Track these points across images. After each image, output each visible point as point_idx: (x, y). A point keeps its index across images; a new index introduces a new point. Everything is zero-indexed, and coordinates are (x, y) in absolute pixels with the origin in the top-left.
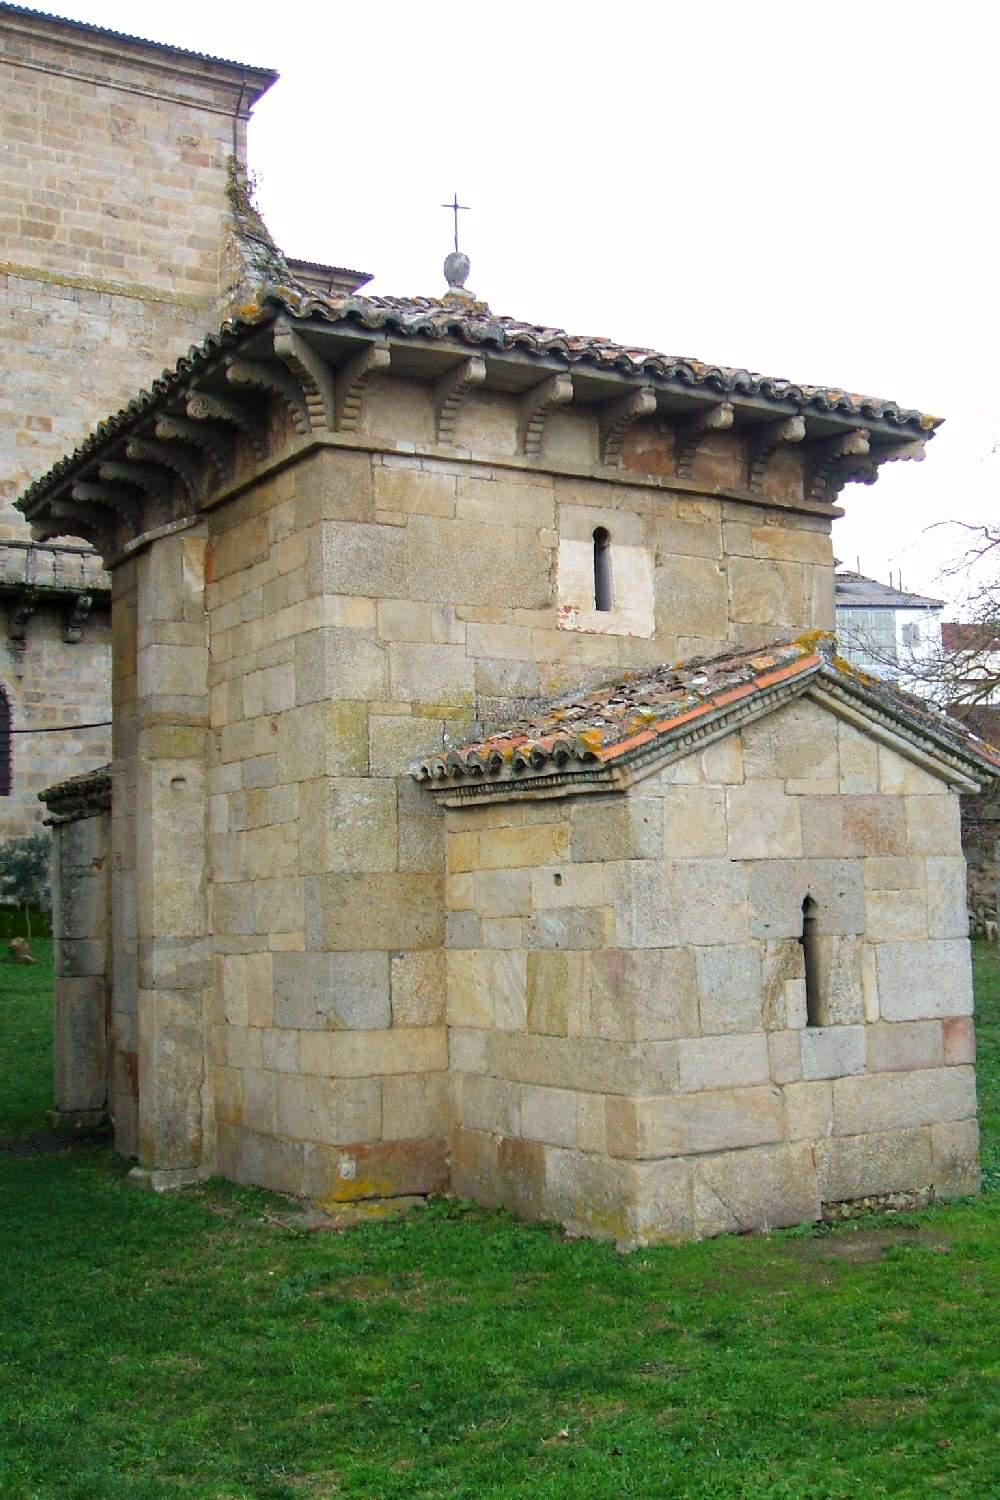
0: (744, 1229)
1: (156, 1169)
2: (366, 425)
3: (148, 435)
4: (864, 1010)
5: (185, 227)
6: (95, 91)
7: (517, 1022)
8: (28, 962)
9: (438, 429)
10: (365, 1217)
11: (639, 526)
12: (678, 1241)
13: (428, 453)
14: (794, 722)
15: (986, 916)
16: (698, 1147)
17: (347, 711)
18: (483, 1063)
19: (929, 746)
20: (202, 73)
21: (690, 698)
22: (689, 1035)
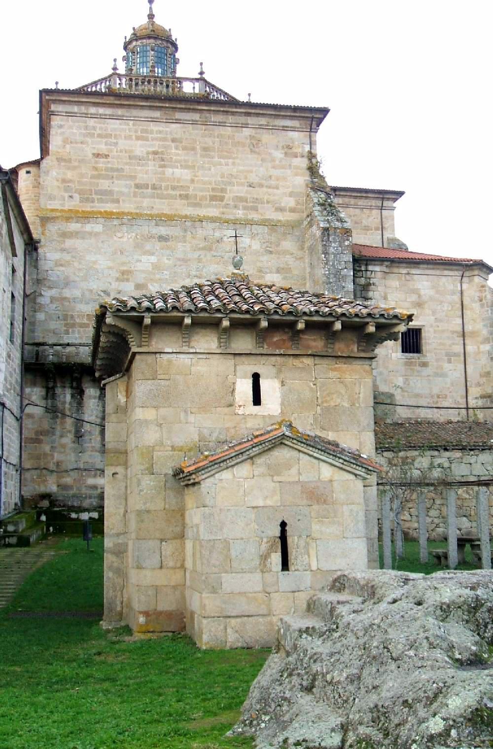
2: (153, 343)
4: (310, 566)
5: (287, 188)
6: (242, 131)
11: (274, 370)
16: (229, 614)
17: (145, 451)
19: (341, 461)
20: (292, 114)
22: (226, 572)
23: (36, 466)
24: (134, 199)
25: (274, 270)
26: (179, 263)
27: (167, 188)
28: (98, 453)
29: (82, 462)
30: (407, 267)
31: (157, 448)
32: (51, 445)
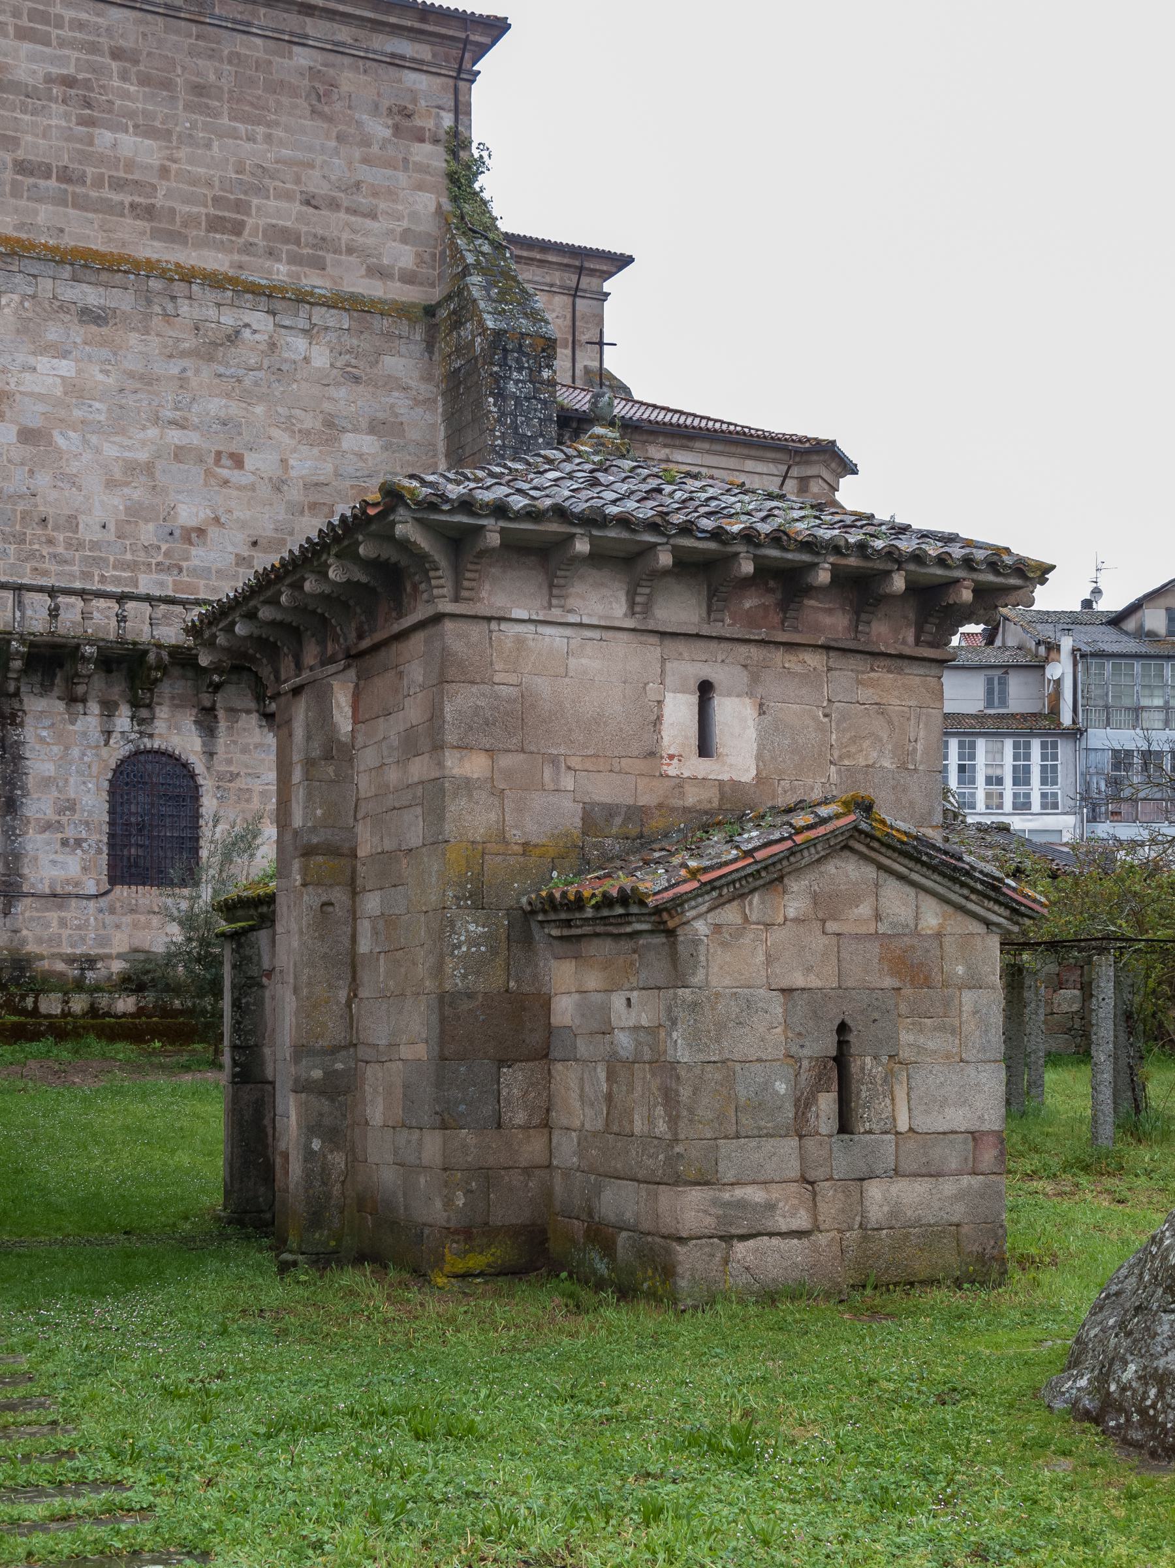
2: (484, 594)
6: (290, 53)
9: (551, 595)
11: (744, 677)
13: (541, 618)
14: (833, 871)
24: (13, 201)
25: (364, 425)
26: (131, 384)
27: (98, 183)
30: (665, 446)
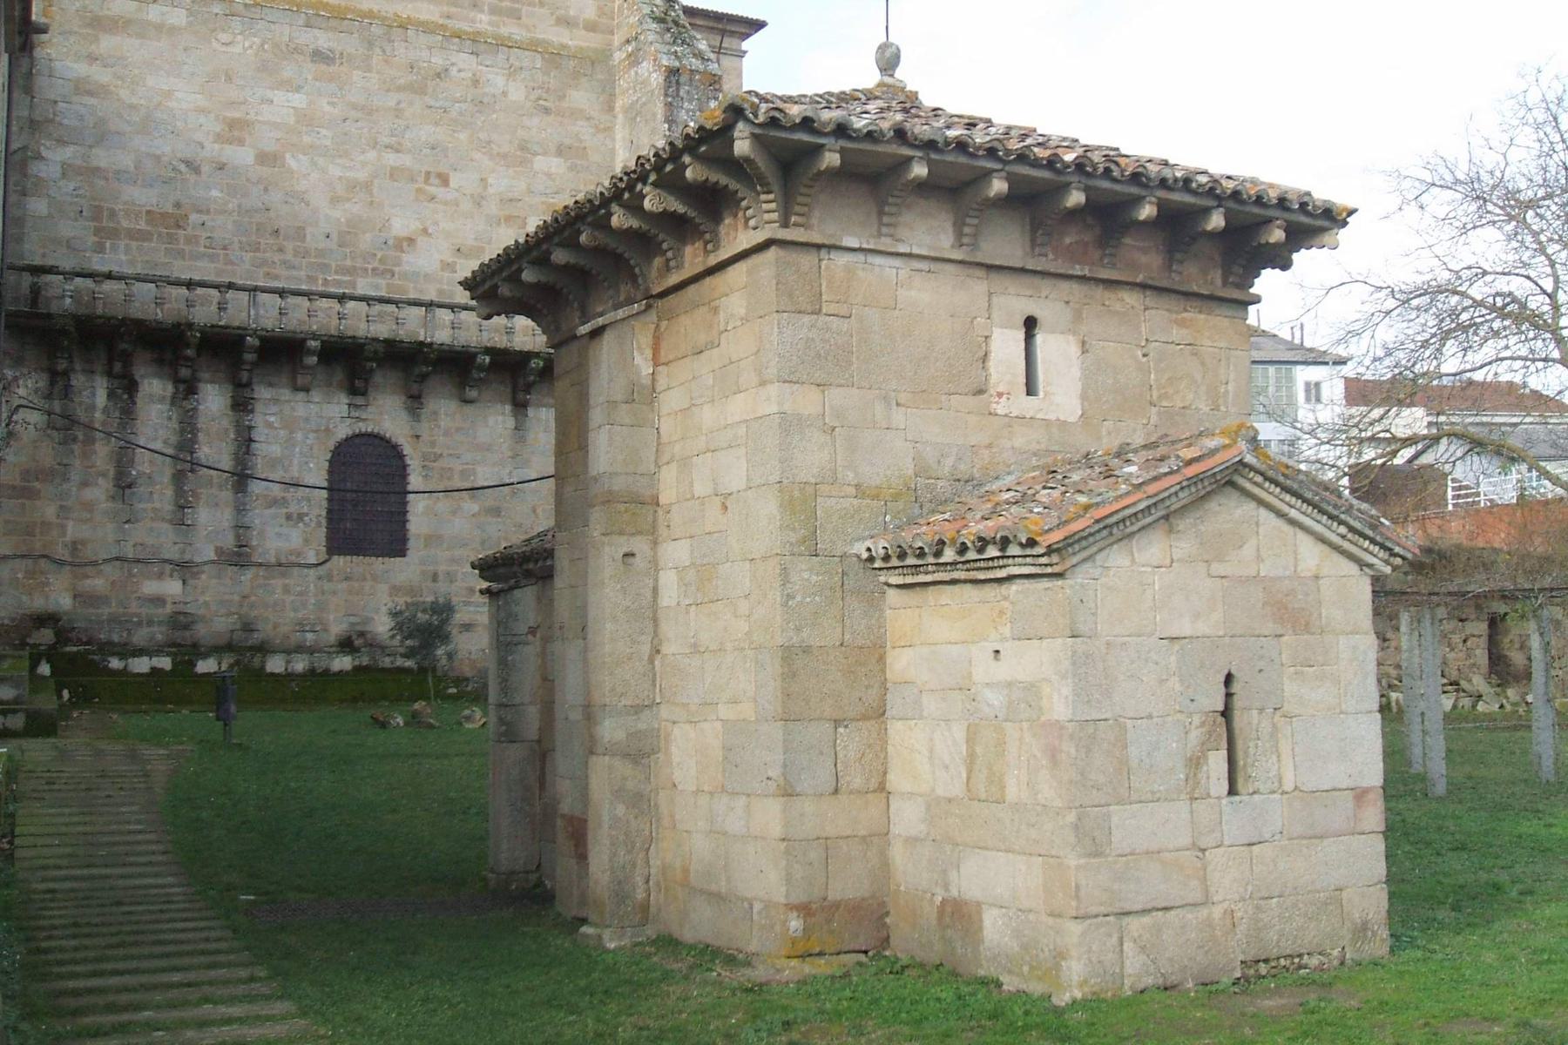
0: (1168, 984)
1: (607, 927)
2: (814, 221)
3: (603, 225)
7: (957, 789)
8: (431, 727)
9: (881, 224)
10: (813, 972)
12: (1110, 994)
15: (1390, 686)
16: (1128, 907)
17: (797, 494)
18: (923, 827)
19: (1343, 530)
21: (1124, 486)
23: (23, 550)
26: (353, 114)
28: (166, 526)
29: (132, 543)
31: (824, 488)
32: (59, 503)
